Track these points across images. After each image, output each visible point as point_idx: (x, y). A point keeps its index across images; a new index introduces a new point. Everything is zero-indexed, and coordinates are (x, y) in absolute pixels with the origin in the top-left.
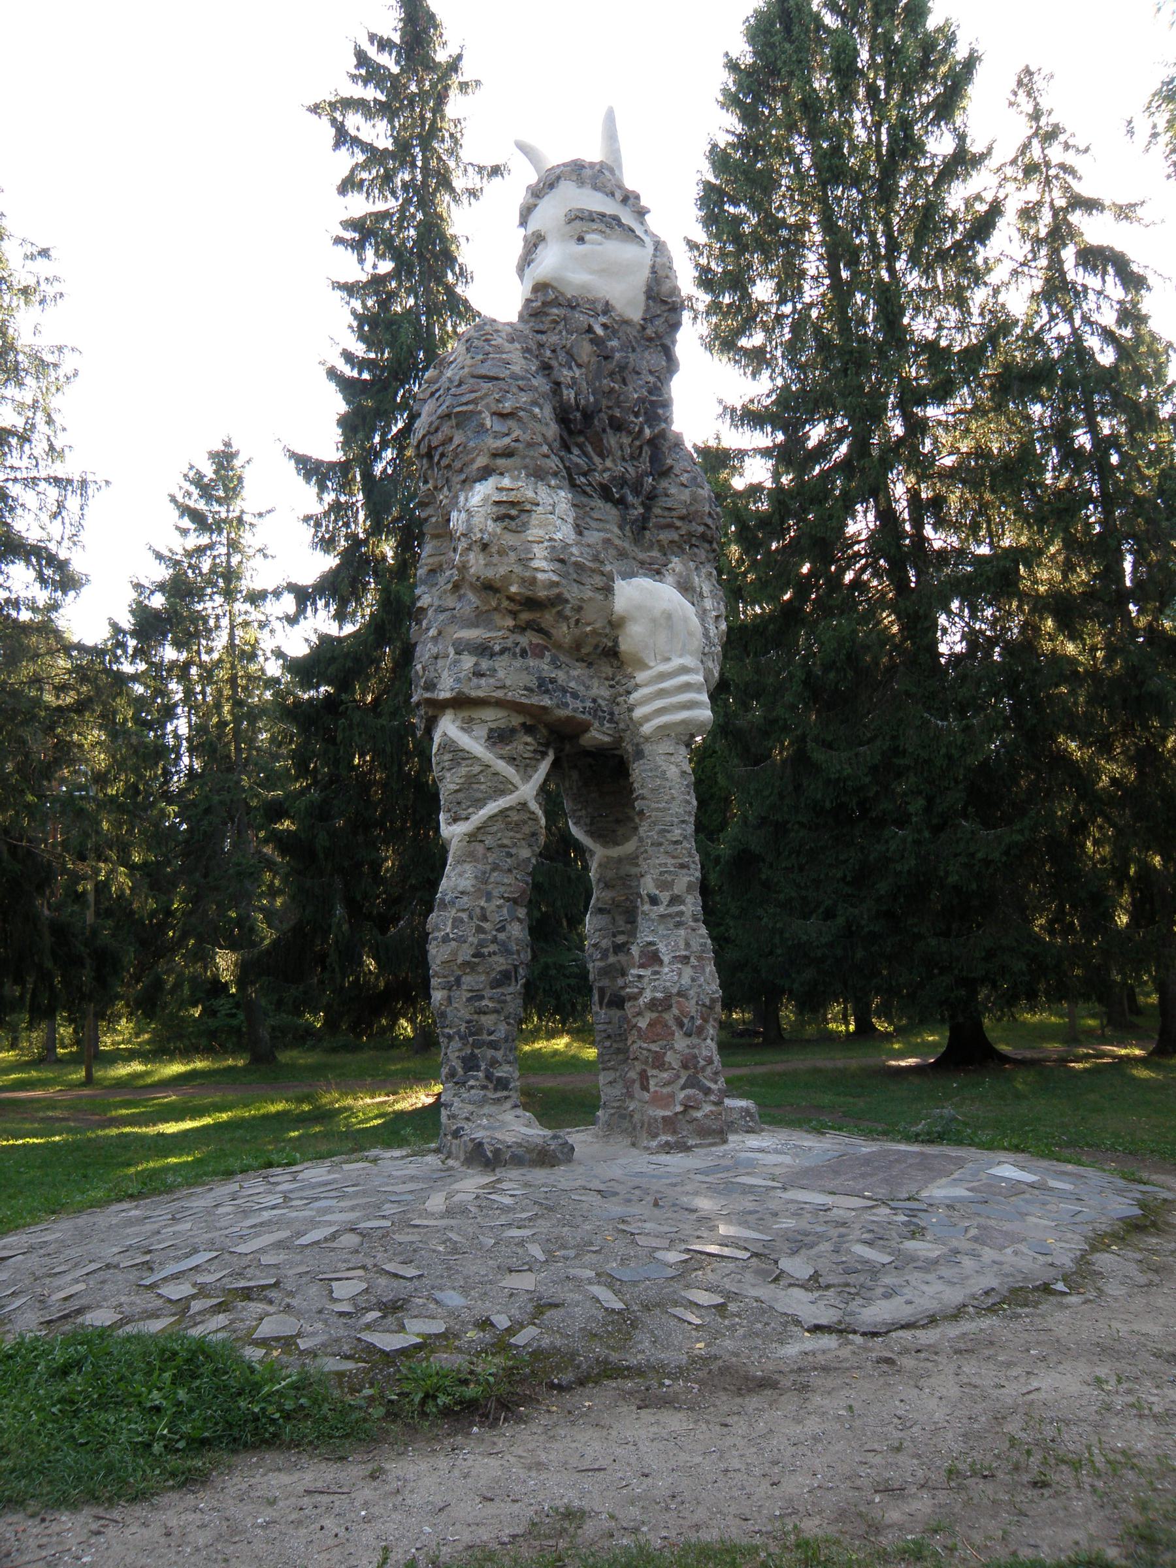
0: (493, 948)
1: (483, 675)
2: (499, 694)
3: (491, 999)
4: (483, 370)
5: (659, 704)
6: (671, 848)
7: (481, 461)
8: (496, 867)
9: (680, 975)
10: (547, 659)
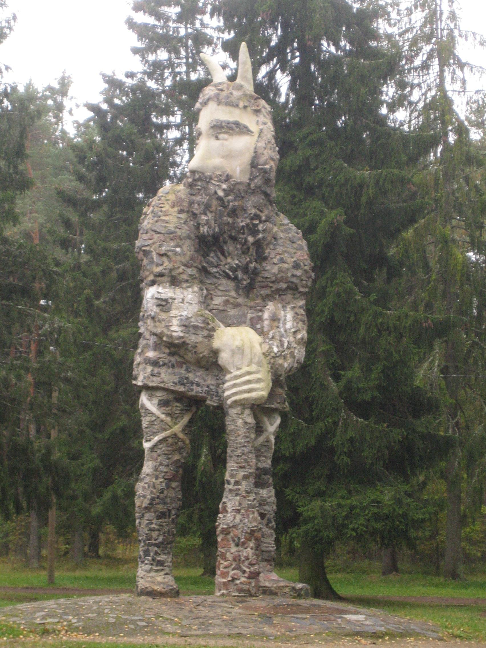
0: (157, 501)
1: (155, 376)
2: (162, 385)
3: (156, 524)
4: (155, 228)
5: (234, 390)
6: (236, 459)
7: (151, 278)
8: (161, 464)
9: (234, 518)
10: (184, 368)
